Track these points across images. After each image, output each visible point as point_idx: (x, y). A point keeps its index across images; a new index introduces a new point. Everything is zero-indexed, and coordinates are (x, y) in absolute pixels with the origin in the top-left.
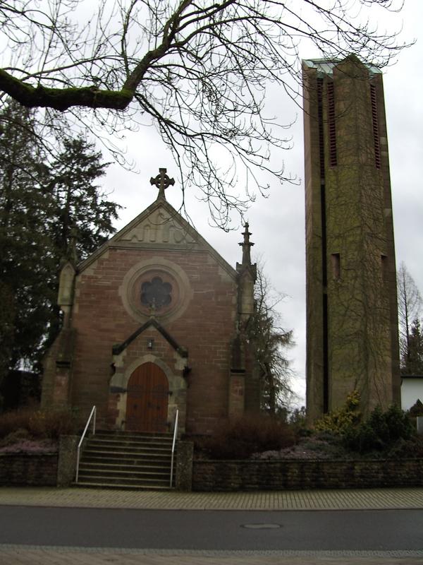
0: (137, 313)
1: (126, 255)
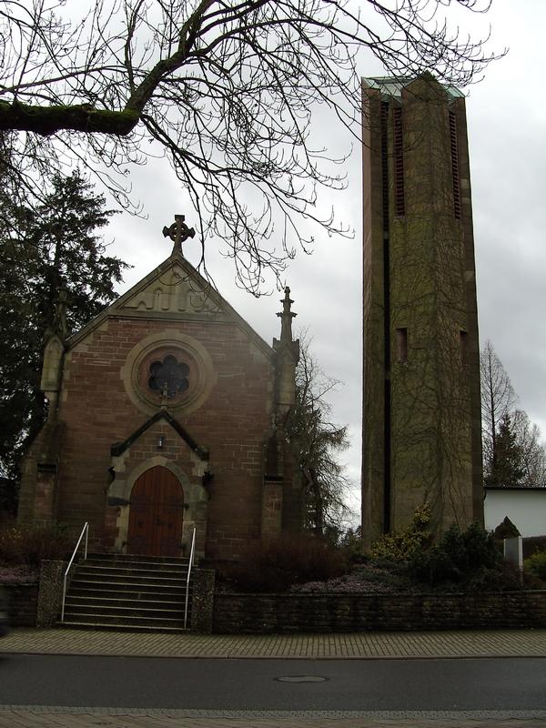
0: (144, 403)
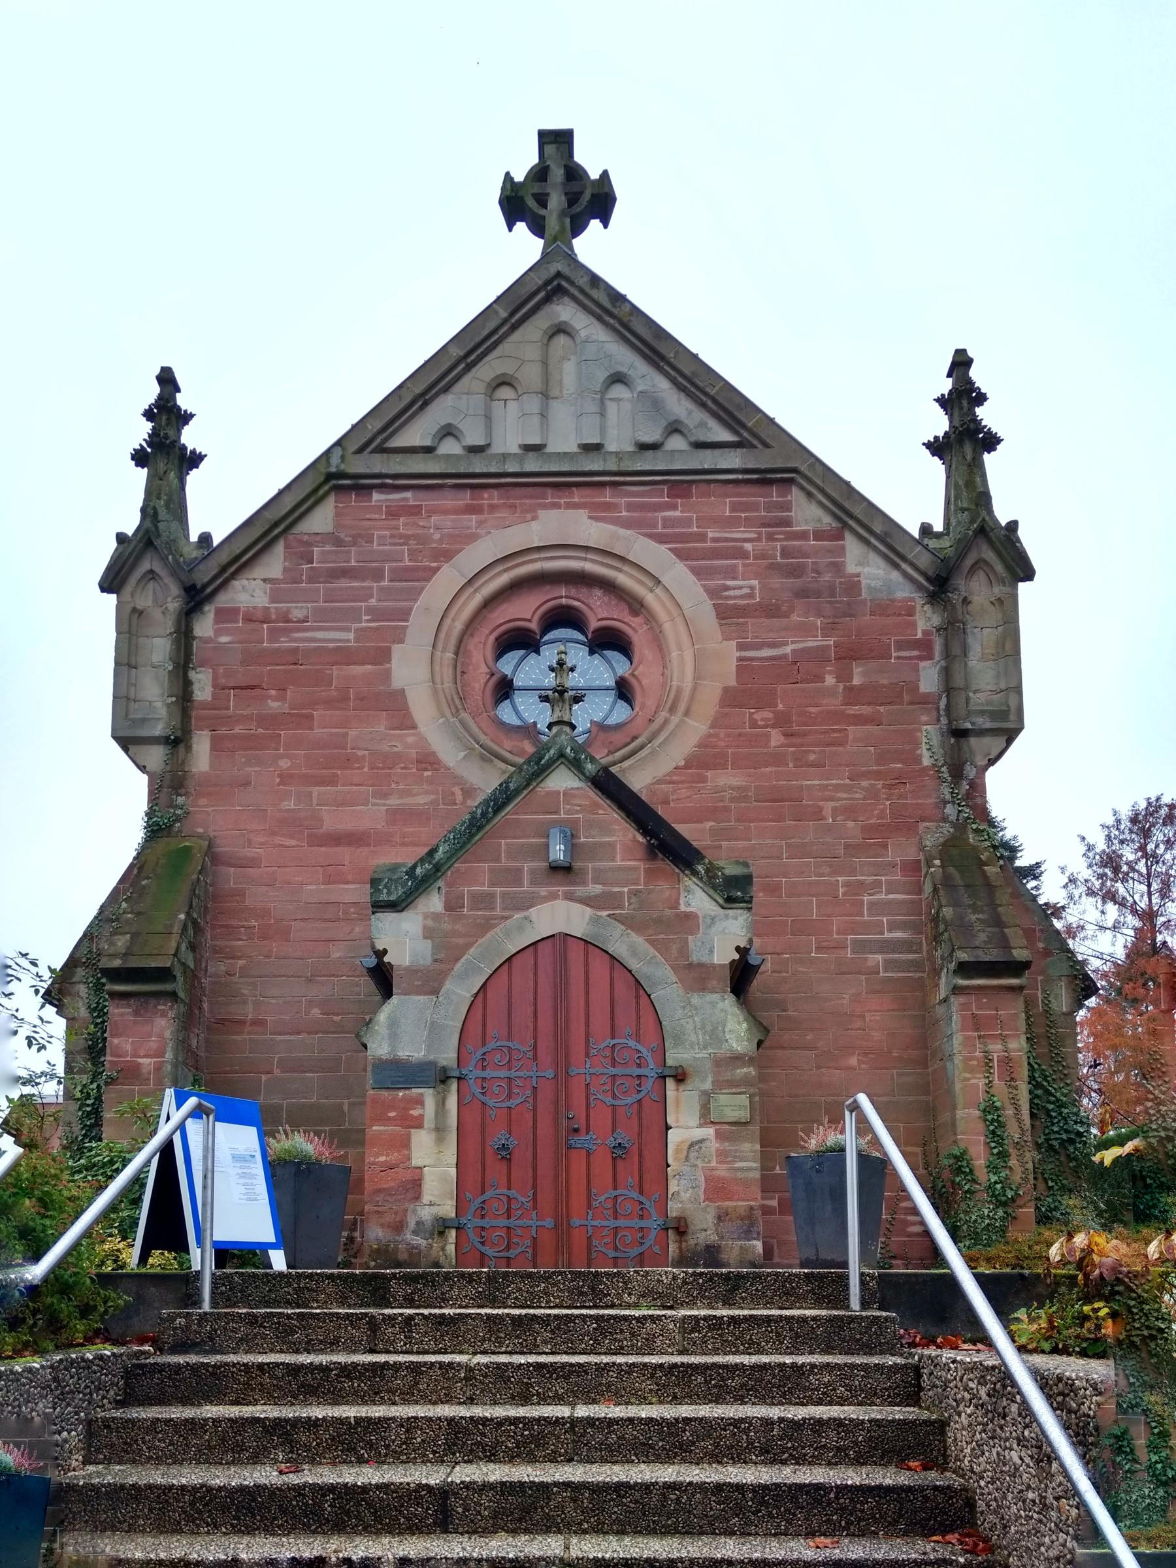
0: (483, 758)
1: (415, 511)
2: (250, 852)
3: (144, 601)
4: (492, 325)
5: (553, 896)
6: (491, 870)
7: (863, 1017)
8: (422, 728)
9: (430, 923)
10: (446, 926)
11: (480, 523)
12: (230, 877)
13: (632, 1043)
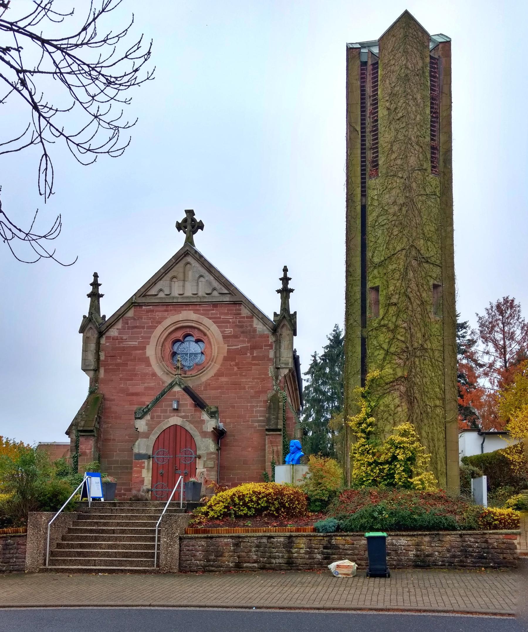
0: (167, 374)
1: (152, 311)
2: (112, 398)
3: (89, 335)
4: (171, 264)
5: (174, 416)
6: (161, 410)
7: (252, 439)
8: (153, 366)
9: (147, 422)
10: (151, 423)
11: (168, 314)
12: (108, 404)
13: (190, 450)
